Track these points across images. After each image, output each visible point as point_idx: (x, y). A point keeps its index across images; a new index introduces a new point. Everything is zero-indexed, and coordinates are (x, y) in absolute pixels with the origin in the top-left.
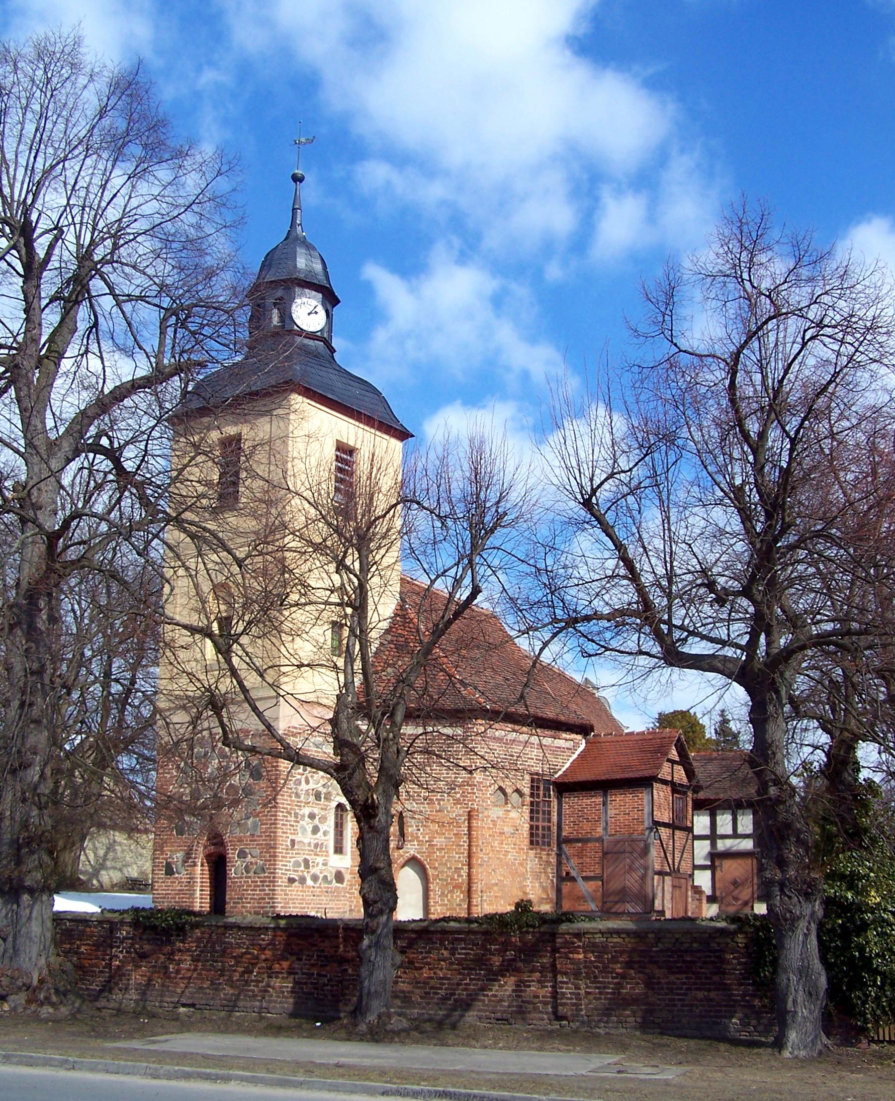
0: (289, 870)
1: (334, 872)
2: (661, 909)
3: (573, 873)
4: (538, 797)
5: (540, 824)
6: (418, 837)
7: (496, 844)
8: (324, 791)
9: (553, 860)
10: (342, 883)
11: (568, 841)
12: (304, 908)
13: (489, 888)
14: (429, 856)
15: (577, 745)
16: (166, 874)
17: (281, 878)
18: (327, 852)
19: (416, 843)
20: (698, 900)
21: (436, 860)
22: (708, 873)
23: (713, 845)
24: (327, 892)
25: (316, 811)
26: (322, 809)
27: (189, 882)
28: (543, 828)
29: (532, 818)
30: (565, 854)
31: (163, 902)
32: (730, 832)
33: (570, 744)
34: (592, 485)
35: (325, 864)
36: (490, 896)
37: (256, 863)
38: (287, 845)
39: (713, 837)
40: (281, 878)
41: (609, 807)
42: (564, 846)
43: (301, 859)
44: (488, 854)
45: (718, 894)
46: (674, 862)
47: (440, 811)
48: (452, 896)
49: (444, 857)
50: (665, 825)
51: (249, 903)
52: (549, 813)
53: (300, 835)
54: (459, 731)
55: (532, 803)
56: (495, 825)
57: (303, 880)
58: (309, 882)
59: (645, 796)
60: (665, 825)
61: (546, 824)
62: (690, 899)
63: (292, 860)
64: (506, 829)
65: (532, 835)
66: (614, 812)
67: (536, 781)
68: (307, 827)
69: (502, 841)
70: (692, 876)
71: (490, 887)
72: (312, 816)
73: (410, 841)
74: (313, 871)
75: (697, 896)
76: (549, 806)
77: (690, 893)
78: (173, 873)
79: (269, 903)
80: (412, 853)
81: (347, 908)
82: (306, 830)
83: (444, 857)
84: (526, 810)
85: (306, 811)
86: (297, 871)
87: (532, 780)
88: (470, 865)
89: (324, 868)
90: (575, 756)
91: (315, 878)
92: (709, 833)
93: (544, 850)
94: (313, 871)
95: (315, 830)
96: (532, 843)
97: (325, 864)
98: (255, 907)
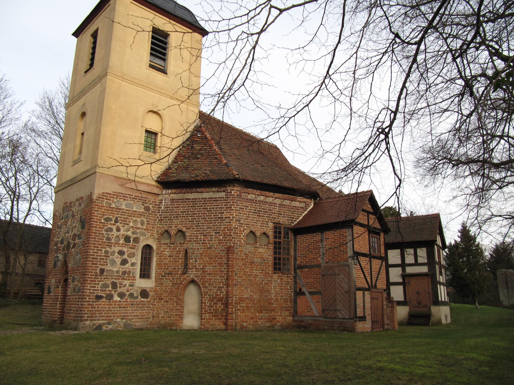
0: (98, 290)
1: (139, 291)
2: (362, 315)
3: (304, 289)
4: (280, 237)
5: (282, 256)
6: (196, 266)
7: (248, 270)
8: (133, 236)
9: (291, 281)
10: (147, 298)
11: (301, 267)
12: (111, 316)
13: (242, 301)
14: (202, 279)
15: (307, 206)
17: (89, 296)
18: (134, 277)
19: (194, 270)
20: (391, 307)
21: (207, 282)
22: (401, 287)
23: (404, 270)
24: (132, 304)
25: (125, 249)
26: (131, 248)
28: (284, 259)
29: (275, 253)
30: (299, 276)
32: (413, 261)
33: (302, 205)
35: (132, 285)
36: (243, 306)
38: (97, 273)
39: (403, 265)
40: (89, 296)
42: (298, 271)
43: (109, 282)
44: (241, 277)
45: (408, 300)
46: (371, 281)
47: (210, 248)
48: (216, 307)
49: (212, 279)
50: (364, 255)
52: (288, 249)
53: (109, 265)
54: (223, 194)
55: (275, 243)
56: (247, 257)
57: (110, 297)
58: (116, 298)
59: (347, 232)
60: (364, 255)
61: (286, 256)
62: (385, 307)
63: (101, 283)
64: (255, 260)
65: (275, 264)
67: (277, 228)
68: (117, 260)
69: (253, 267)
70: (451, 247)
71: (242, 300)
72: (121, 253)
73: (191, 269)
74: (119, 290)
75: (390, 305)
76: (288, 244)
77: (385, 303)
80: (192, 277)
81: (151, 315)
82: (115, 262)
83: (212, 279)
84: (271, 246)
85: (117, 249)
86: (105, 291)
87: (275, 228)
88: (228, 285)
89: (130, 288)
90: (306, 213)
91: (121, 295)
92: (398, 251)
93: (285, 274)
94: (119, 290)
95: (124, 262)
96: (275, 269)
97: (132, 285)
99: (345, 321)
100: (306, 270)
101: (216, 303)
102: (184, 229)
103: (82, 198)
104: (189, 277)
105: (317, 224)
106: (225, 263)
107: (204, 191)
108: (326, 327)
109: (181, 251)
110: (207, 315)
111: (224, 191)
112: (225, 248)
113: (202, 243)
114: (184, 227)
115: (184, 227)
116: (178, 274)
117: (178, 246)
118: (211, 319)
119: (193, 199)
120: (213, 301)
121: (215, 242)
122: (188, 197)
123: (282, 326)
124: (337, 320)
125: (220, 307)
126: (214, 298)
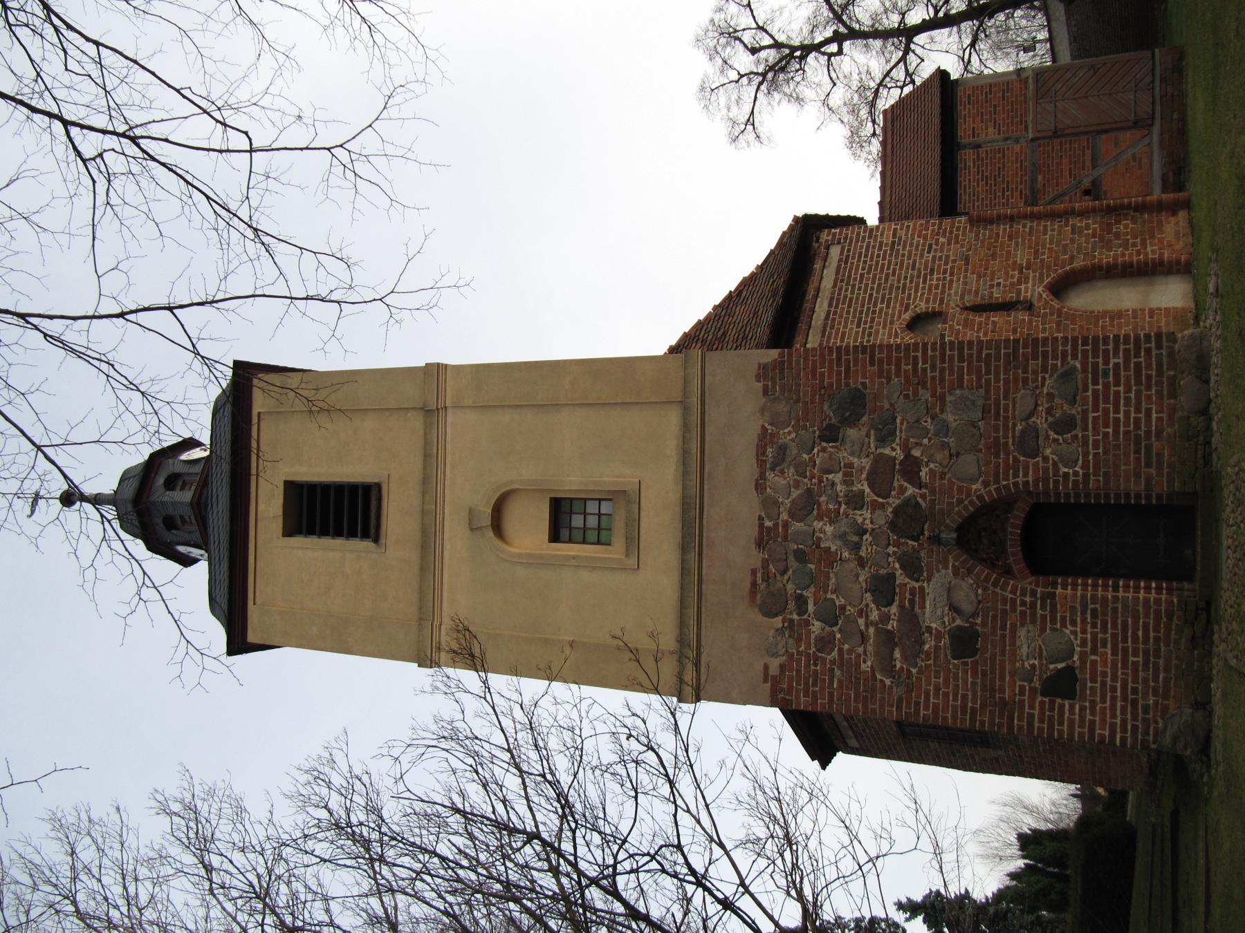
6: (1012, 284)
16: (1071, 695)
19: (1023, 287)
21: (1057, 258)
27: (1094, 613)
31: (1146, 709)
34: (142, 137)
37: (1051, 396)
41: (983, 138)
48: (1127, 234)
51: (1148, 411)
66: (991, 130)
78: (1070, 670)
79: (1148, 351)
80: (1041, 289)
98: (1159, 394)
99: (1158, 72)
100: (1040, 178)
101: (1117, 236)
102: (907, 316)
103: (765, 439)
104: (1040, 295)
105: (938, 175)
106: (1011, 227)
107: (816, 284)
108: (1175, 116)
109: (966, 320)
110: (1149, 249)
111: (828, 248)
112: (971, 231)
113: (952, 274)
114: (899, 317)
115: (899, 317)
116: (1030, 321)
117: (951, 327)
118: (1161, 241)
119: (830, 305)
120: (1110, 241)
121: (953, 251)
122: (823, 315)
123: (1174, 214)
124: (1157, 89)
125: (1126, 227)
126: (1102, 240)
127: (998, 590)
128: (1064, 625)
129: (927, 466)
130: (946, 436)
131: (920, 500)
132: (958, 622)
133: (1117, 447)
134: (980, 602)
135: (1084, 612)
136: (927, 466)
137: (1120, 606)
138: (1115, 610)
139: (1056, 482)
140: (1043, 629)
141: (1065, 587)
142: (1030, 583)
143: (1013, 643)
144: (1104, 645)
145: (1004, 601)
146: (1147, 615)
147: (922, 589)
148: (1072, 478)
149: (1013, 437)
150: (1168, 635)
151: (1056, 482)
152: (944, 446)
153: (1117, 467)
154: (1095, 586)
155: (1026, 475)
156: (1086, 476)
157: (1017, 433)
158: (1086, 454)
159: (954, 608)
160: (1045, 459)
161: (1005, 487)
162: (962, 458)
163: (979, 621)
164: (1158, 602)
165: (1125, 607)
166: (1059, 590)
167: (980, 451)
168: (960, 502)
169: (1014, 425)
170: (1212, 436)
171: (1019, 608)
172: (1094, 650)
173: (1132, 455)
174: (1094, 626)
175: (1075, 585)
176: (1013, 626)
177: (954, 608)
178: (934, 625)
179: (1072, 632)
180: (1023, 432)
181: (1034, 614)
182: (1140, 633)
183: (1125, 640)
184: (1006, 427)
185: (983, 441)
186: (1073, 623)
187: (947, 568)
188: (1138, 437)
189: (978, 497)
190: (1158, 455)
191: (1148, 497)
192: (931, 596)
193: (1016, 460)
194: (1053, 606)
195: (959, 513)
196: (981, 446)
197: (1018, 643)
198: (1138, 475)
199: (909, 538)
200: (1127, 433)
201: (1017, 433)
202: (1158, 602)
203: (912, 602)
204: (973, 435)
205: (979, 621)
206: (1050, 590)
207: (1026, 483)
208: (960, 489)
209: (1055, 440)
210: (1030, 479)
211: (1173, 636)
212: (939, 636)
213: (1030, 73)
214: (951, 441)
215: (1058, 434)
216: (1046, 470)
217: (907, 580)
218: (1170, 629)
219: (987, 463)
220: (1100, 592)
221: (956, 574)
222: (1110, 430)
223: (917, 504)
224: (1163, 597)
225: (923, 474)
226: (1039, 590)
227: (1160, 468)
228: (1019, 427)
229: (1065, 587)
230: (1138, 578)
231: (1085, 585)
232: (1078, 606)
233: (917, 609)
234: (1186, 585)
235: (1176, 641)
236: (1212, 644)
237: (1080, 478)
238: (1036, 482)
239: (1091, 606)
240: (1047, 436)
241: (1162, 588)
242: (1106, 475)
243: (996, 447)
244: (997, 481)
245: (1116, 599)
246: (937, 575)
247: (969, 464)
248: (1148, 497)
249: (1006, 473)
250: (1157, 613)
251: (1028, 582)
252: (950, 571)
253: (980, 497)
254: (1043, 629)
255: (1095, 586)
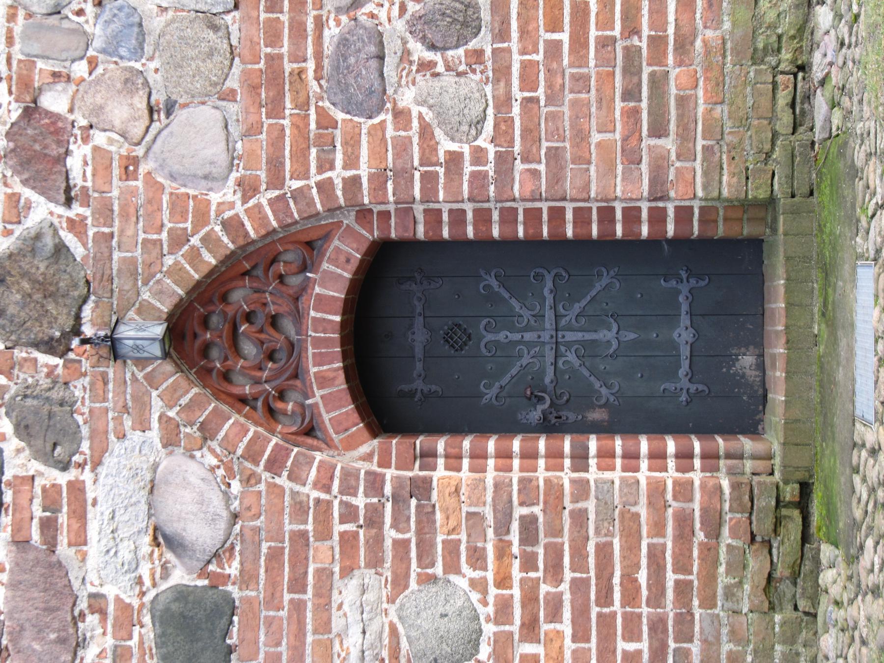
127: (282, 480)
128: (452, 567)
129: (86, 139)
130: (138, 51)
131: (69, 239)
132: (180, 576)
133: (581, 82)
134: (235, 516)
135: (502, 528)
136: (86, 139)
137: (591, 505)
138: (580, 518)
139: (429, 179)
140: (400, 583)
141: (454, 460)
142: (368, 457)
143: (324, 626)
144: (555, 615)
145: (300, 509)
146: (658, 528)
147: (77, 489)
148: (468, 168)
149: (319, 56)
150: (709, 578)
151: (429, 179)
152: (133, 81)
153: (581, 137)
154: (530, 455)
155: (351, 162)
156: (504, 161)
157: (328, 47)
158: (504, 103)
159: (163, 538)
160: (401, 116)
161: (298, 195)
162: (181, 116)
163: (233, 569)
164: (684, 491)
165: (605, 505)
166: (440, 473)
167: (229, 96)
168: (179, 240)
169: (320, 24)
170: (813, 46)
171: (338, 528)
172: (530, 629)
173: (619, 105)
174: (529, 563)
175: (478, 456)
176: (324, 575)
177: (163, 538)
178: (110, 591)
179: (474, 584)
180: (343, 42)
181: (377, 542)
182: (642, 576)
183: (605, 598)
184: (298, 30)
185: (237, 69)
186: (477, 558)
187: (143, 426)
188: (632, 54)
189: (225, 224)
190: (682, 101)
191: (657, 217)
192: (104, 508)
193: (326, 122)
194: (426, 517)
195: (176, 272)
196: (233, 83)
197: (337, 624)
198: (633, 159)
199: (37, 345)
200: (606, 43)
201: (328, 47)
202: (684, 491)
203: (49, 526)
204: (210, 54)
205: (233, 569)
206: (416, 472)
207: (352, 184)
208: (178, 204)
209: (426, 66)
210: (364, 171)
211: (723, 579)
212: (126, 619)
213: (304, 19)
214: (151, 67)
215: (432, 47)
216: (403, 147)
217: (35, 466)
218: (716, 563)
219: (252, 131)
220: (542, 474)
221: (170, 441)
222: (564, 37)
223: (61, 249)
224: (696, 477)
225: (74, 163)
226: (390, 473)
227: (686, 135)
228: (331, 32)
229: (454, 460)
230: (631, 430)
231: (504, 455)
232: (488, 512)
233: (64, 550)
234: (747, 444)
235: (729, 593)
236: (815, 593)
237: (490, 168)
238: (378, 180)
239: (519, 511)
240: (406, 53)
241: (663, 456)
242: (554, 155)
243: (272, 86)
244: (276, 180)
245: (581, 489)
246: (116, 446)
247: (200, 135)
248: (657, 217)
249: (301, 155)
250: (684, 522)
251: (363, 453)
252: (154, 434)
253: (232, 226)
254: (400, 583)
255: (530, 455)
